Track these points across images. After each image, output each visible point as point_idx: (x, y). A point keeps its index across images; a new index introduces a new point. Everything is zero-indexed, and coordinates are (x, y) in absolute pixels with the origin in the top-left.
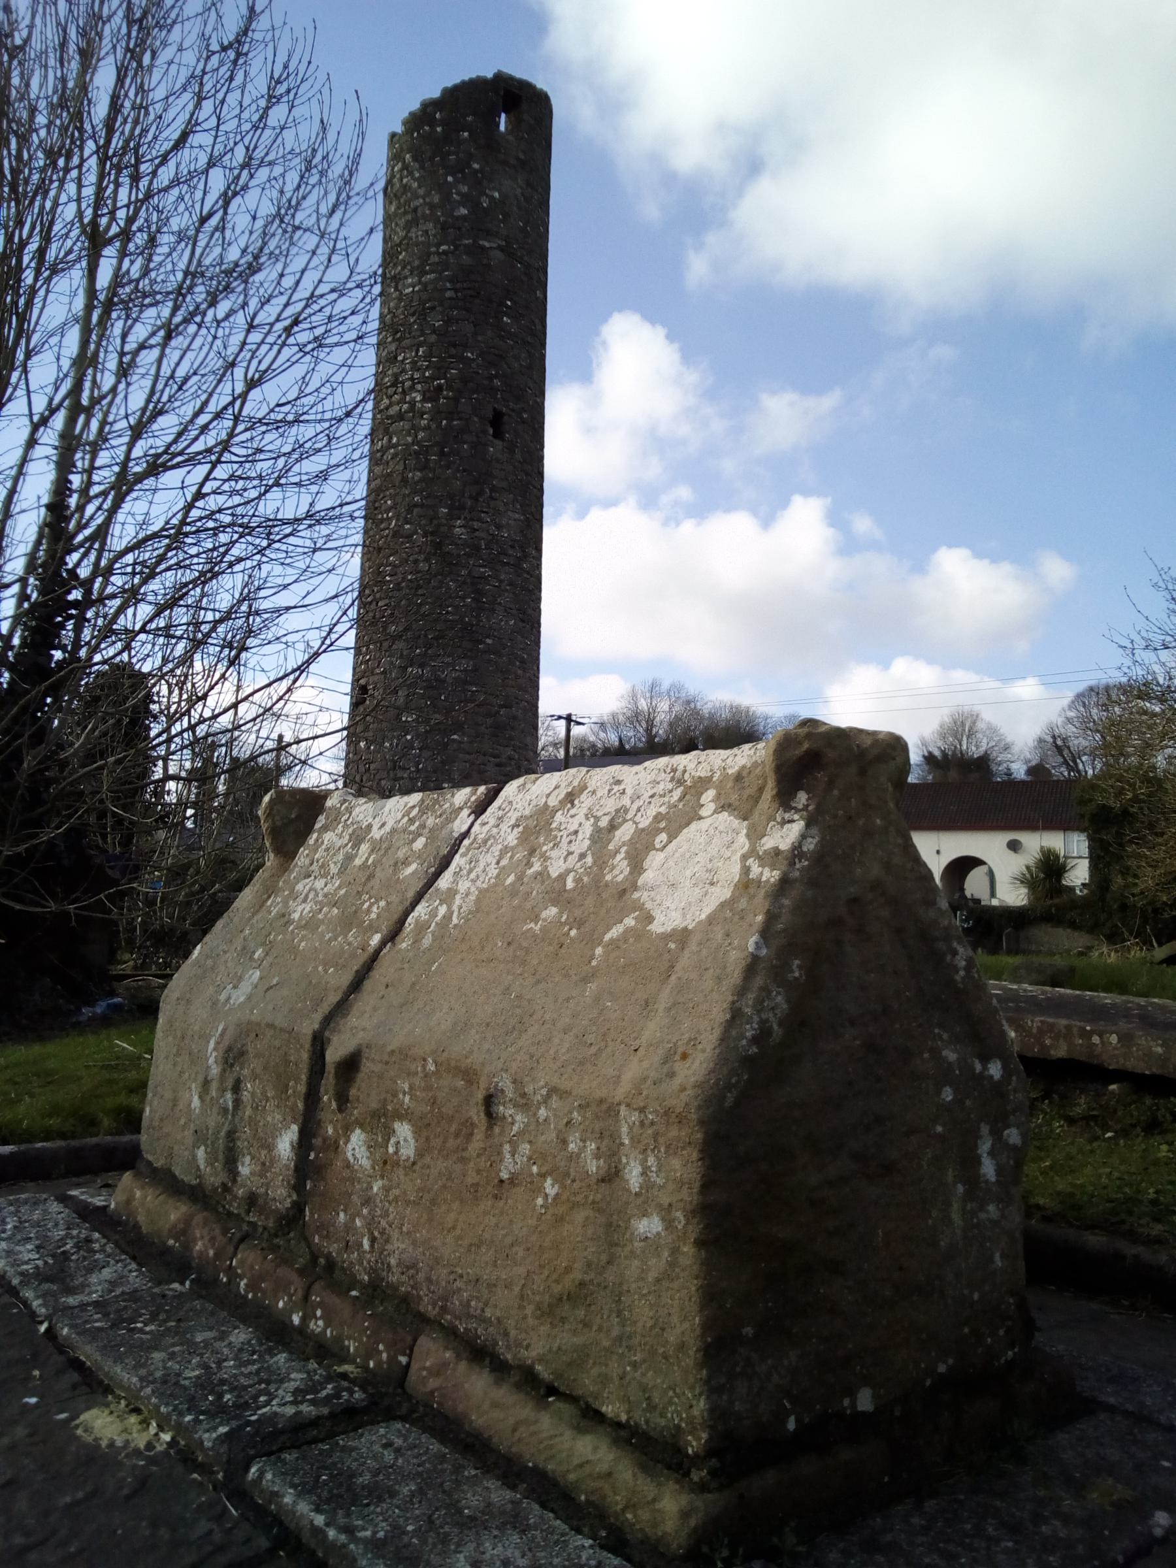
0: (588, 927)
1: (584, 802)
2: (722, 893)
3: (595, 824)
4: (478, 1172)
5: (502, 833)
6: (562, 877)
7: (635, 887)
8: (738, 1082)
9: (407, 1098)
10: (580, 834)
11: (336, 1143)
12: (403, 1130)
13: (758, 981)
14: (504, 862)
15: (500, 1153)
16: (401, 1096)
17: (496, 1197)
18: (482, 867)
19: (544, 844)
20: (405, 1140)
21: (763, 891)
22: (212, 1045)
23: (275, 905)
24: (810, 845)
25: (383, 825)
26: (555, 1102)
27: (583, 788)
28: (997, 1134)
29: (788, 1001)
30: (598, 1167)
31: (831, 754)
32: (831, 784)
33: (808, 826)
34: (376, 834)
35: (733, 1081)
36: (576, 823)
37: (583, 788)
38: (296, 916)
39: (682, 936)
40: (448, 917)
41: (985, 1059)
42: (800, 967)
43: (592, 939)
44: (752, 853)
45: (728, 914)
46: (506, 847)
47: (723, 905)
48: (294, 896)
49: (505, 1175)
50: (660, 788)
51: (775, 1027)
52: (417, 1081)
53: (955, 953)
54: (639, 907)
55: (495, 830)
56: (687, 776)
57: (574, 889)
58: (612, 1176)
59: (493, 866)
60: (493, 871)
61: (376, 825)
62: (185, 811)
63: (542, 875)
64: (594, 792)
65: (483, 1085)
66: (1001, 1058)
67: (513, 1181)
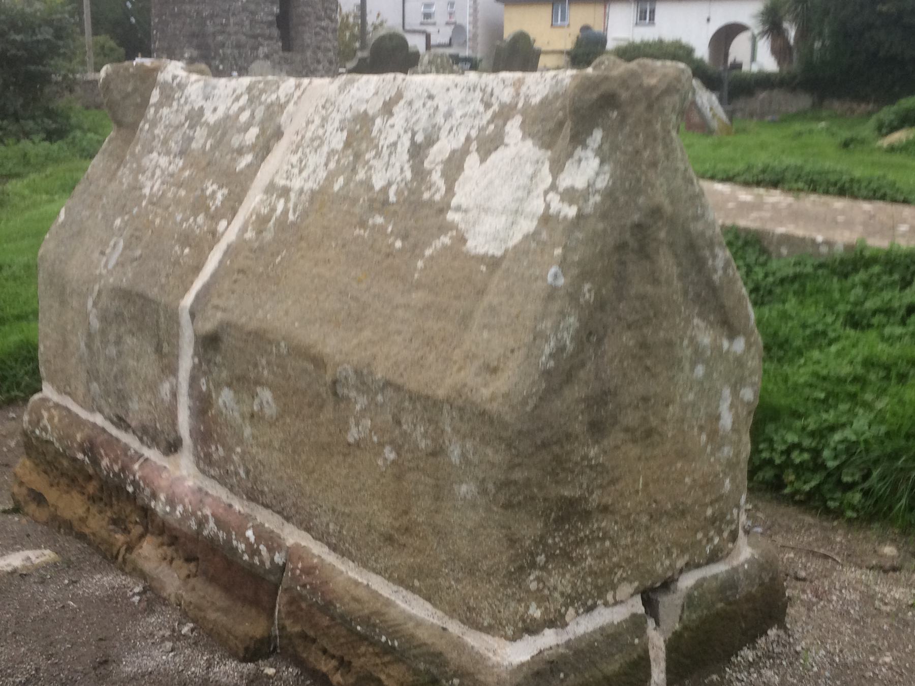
0: (412, 240)
1: (400, 113)
2: (527, 226)
3: (412, 139)
4: (330, 434)
5: (328, 134)
6: (385, 190)
7: (448, 207)
8: (537, 391)
9: (266, 372)
10: (399, 146)
11: (210, 396)
12: (266, 395)
13: (555, 307)
14: (332, 165)
15: (347, 423)
16: (260, 369)
17: (345, 455)
18: (311, 168)
19: (367, 150)
20: (268, 402)
21: (561, 227)
22: (90, 303)
23: (125, 175)
24: (602, 183)
25: (215, 110)
26: (390, 392)
27: (399, 96)
28: (735, 392)
29: (580, 320)
30: (427, 445)
31: (624, 95)
32: (623, 118)
33: (602, 163)
34: (210, 118)
35: (534, 390)
36: (394, 131)
37: (399, 96)
38: (147, 191)
39: (494, 263)
40: (285, 212)
41: (732, 337)
42: (589, 291)
43: (415, 250)
44: (553, 187)
45: (533, 245)
46: (332, 151)
47: (526, 237)
48: (141, 170)
49: (351, 440)
50: (470, 109)
51: (568, 343)
52: (273, 358)
53: (714, 257)
54: (452, 226)
55: (321, 132)
56: (494, 100)
57: (398, 202)
58: (437, 452)
59: (322, 167)
60: (322, 174)
61: (208, 106)
62: (140, 601)
63: (368, 185)
64: (410, 103)
65: (330, 372)
66: (745, 334)
67: (358, 444)
